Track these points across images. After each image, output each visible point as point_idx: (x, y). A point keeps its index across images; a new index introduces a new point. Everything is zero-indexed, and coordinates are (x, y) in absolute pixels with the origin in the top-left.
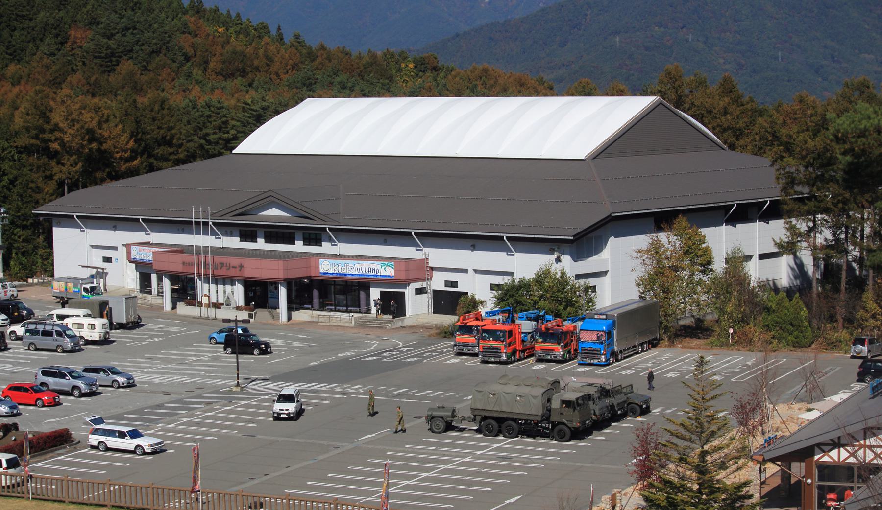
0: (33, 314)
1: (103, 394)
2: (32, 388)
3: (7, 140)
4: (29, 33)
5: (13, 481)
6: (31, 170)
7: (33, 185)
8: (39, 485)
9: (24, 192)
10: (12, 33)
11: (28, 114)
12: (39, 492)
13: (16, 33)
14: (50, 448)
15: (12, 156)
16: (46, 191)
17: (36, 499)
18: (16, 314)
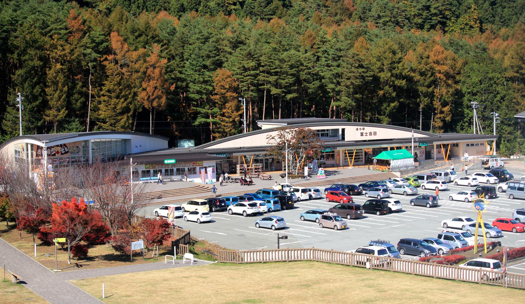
0: (513, 177)
1: (350, 229)
2: (510, 221)
3: (500, 73)
4: (513, 10)
5: (497, 276)
6: (514, 91)
7: (514, 100)
8: (511, 279)
9: (510, 104)
10: (503, 10)
11: (513, 58)
12: (511, 283)
13: (506, 10)
14: (519, 257)
15: (503, 83)
16: (522, 104)
17: (509, 287)
18: (503, 177)
